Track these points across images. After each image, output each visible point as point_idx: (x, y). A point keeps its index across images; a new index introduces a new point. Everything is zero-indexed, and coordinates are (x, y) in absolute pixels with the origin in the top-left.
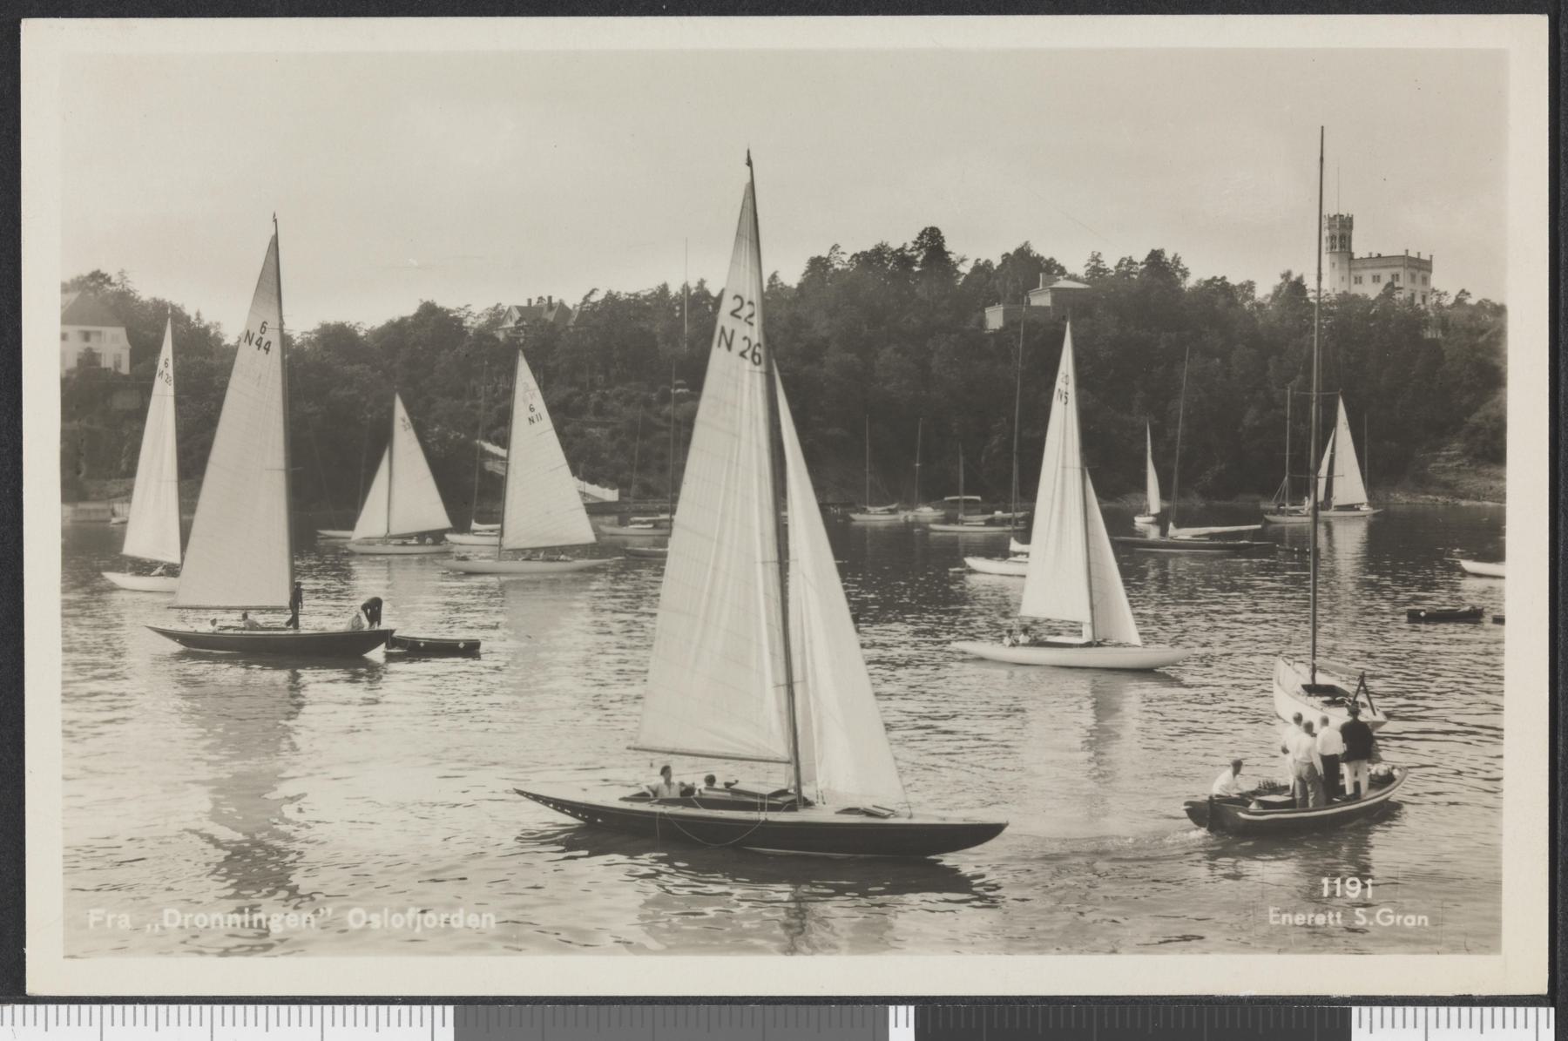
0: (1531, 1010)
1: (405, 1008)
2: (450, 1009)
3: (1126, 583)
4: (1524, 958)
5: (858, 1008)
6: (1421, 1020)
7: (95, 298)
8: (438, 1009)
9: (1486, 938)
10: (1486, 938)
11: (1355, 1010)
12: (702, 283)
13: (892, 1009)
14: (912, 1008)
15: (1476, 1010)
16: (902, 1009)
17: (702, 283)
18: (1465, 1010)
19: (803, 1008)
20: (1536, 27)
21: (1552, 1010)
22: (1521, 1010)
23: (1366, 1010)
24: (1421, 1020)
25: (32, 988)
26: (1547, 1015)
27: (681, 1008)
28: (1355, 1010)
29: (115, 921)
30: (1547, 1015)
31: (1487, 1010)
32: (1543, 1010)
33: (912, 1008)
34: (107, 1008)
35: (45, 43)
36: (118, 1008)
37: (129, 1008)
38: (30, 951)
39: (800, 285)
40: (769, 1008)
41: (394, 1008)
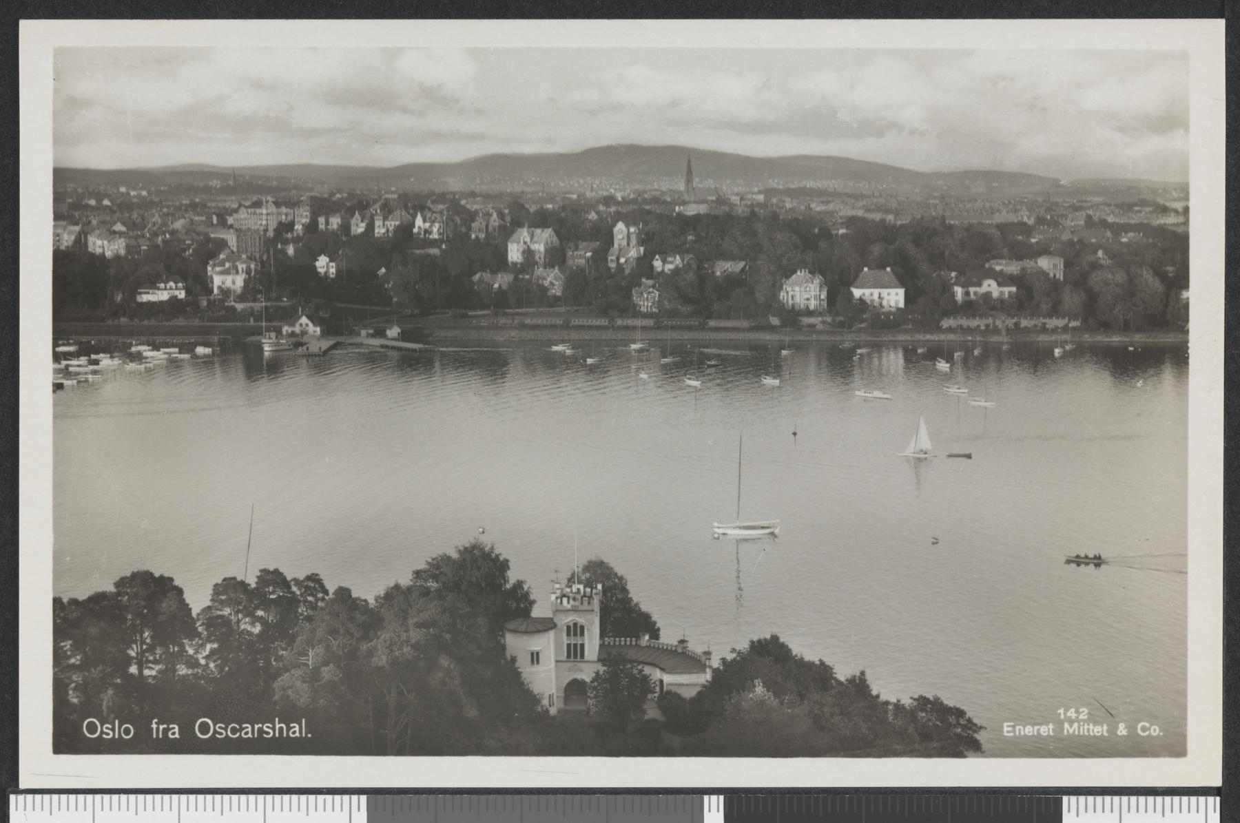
0: (1193, 799)
1: (329, 797)
2: (364, 798)
3: (59, 335)
4: (1205, 760)
8: (355, 797)
9: (1174, 745)
11: (1065, 799)
13: (706, 798)
16: (714, 798)
18: (1150, 799)
20: (1218, 26)
21: (1218, 799)
23: (1073, 799)
25: (22, 786)
26: (1214, 802)
27: (535, 797)
28: (1065, 799)
29: (166, 731)
30: (1214, 802)
32: (1211, 799)
33: (722, 797)
34: (98, 797)
36: (107, 797)
38: (590, 758)
40: (611, 797)
41: (321, 797)
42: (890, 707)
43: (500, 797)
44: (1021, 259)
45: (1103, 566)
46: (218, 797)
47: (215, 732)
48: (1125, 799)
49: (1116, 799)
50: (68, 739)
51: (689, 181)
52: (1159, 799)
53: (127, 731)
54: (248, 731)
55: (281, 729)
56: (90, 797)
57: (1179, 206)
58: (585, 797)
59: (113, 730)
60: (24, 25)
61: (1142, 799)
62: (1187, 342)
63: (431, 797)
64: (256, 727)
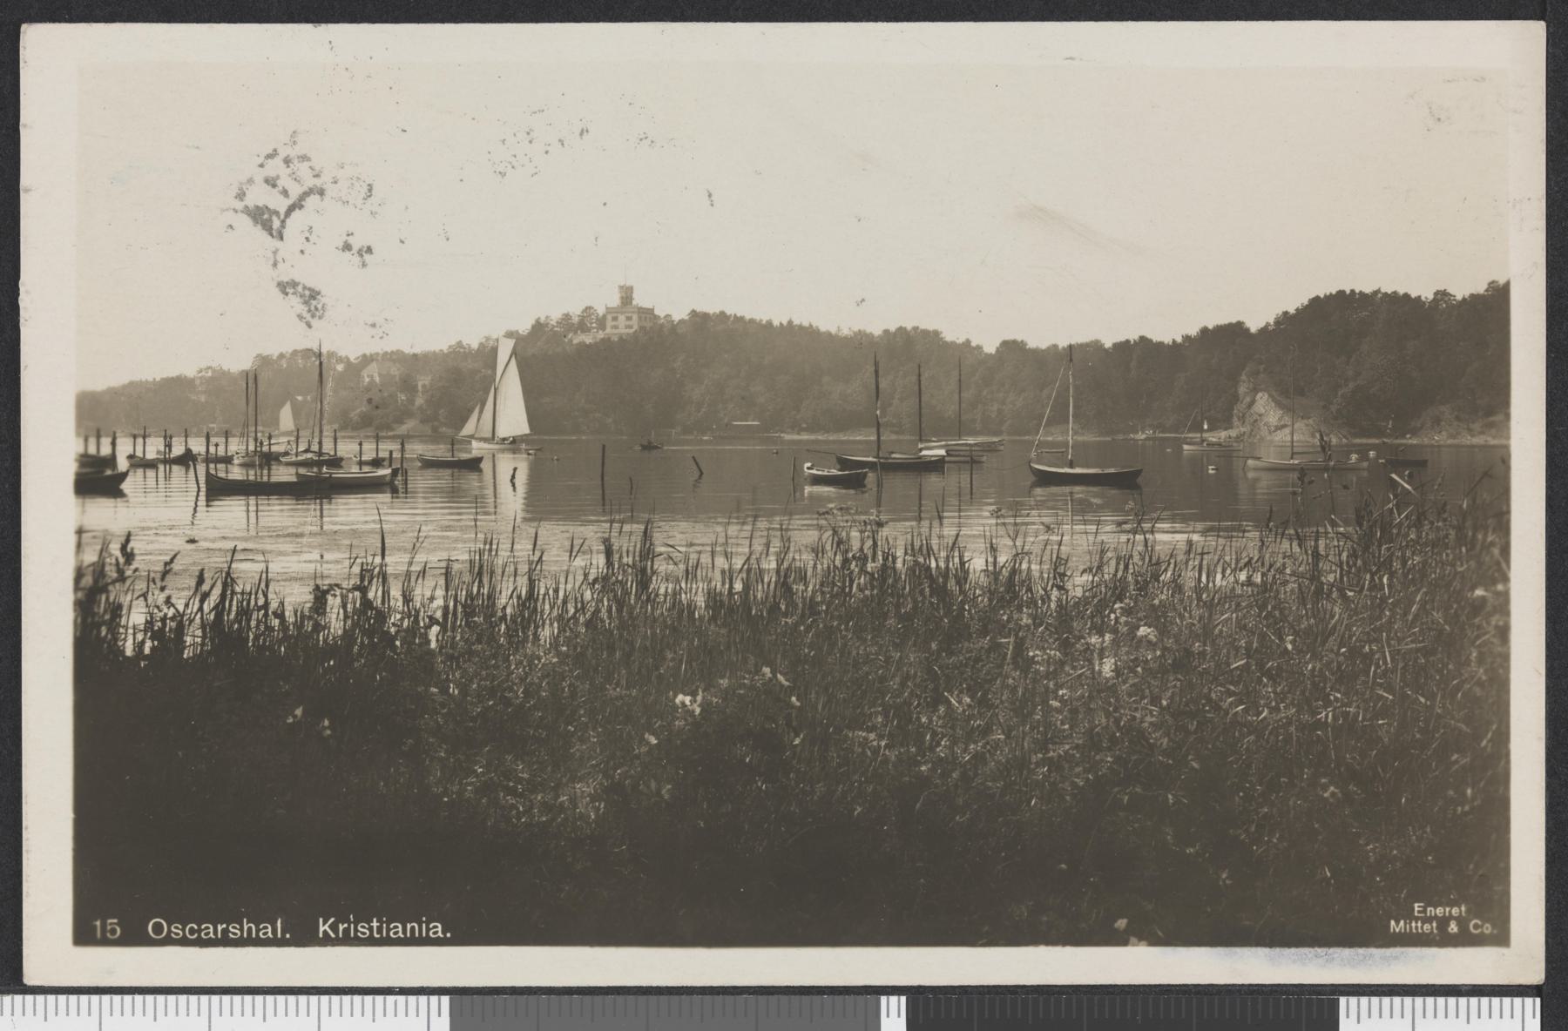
0: (1517, 1001)
1: (401, 999)
2: (446, 1000)
6: (1518, 1012)
7: (94, 412)
8: (434, 999)
9: (1501, 938)
10: (1501, 938)
11: (1343, 1000)
12: (627, 295)
13: (883, 999)
14: (903, 999)
16: (894, 999)
17: (627, 295)
18: (1452, 1000)
19: (795, 999)
21: (1538, 1000)
23: (1353, 1000)
24: (1518, 1012)
25: (30, 978)
26: (1533, 1005)
27: (675, 999)
28: (1343, 1000)
30: (1533, 1005)
32: (1529, 1001)
33: (903, 999)
34: (106, 998)
35: (51, 53)
36: (117, 998)
37: (128, 998)
39: (1264, 331)
41: (391, 999)
42: (1500, 587)
43: (784, 999)
44: (1231, 416)
45: (341, 245)
46: (259, 998)
48: (1419, 1000)
49: (1408, 1000)
52: (1463, 1000)
54: (234, 931)
55: (250, 929)
56: (95, 998)
58: (729, 999)
61: (1441, 1000)
63: (531, 998)
64: (219, 928)
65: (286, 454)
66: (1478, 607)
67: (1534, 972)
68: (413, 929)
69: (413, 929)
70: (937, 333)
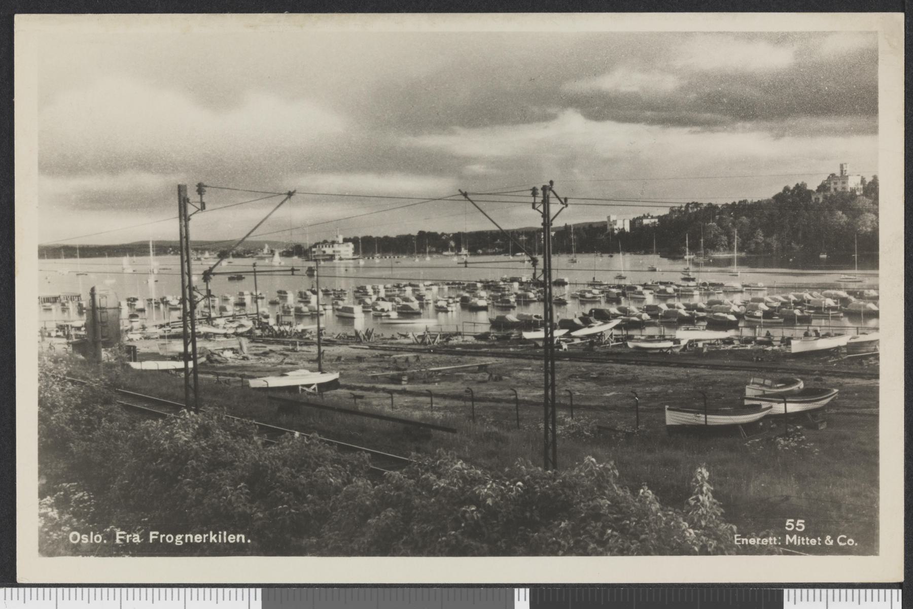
1: (233, 590)
2: (259, 590)
4: (889, 559)
5: (496, 590)
6: (824, 597)
8: (252, 590)
9: (867, 543)
10: (867, 543)
11: (786, 591)
13: (516, 590)
14: (528, 590)
15: (856, 591)
16: (522, 590)
18: (850, 591)
21: (900, 591)
22: (843, 591)
23: (792, 591)
24: (824, 597)
25: (20, 579)
26: (897, 594)
28: (786, 591)
30: (897, 594)
31: (863, 591)
32: (895, 591)
33: (528, 590)
34: (60, 590)
41: (227, 590)
43: (458, 590)
46: (150, 590)
47: (81, 539)
49: (824, 591)
50: (49, 548)
51: (184, 217)
53: (98, 539)
57: (873, 293)
59: (89, 538)
60: (18, 18)
62: (378, 238)
65: (252, 294)
66: (677, 496)
67: (899, 576)
68: (189, 538)
69: (189, 538)
70: (745, 201)
